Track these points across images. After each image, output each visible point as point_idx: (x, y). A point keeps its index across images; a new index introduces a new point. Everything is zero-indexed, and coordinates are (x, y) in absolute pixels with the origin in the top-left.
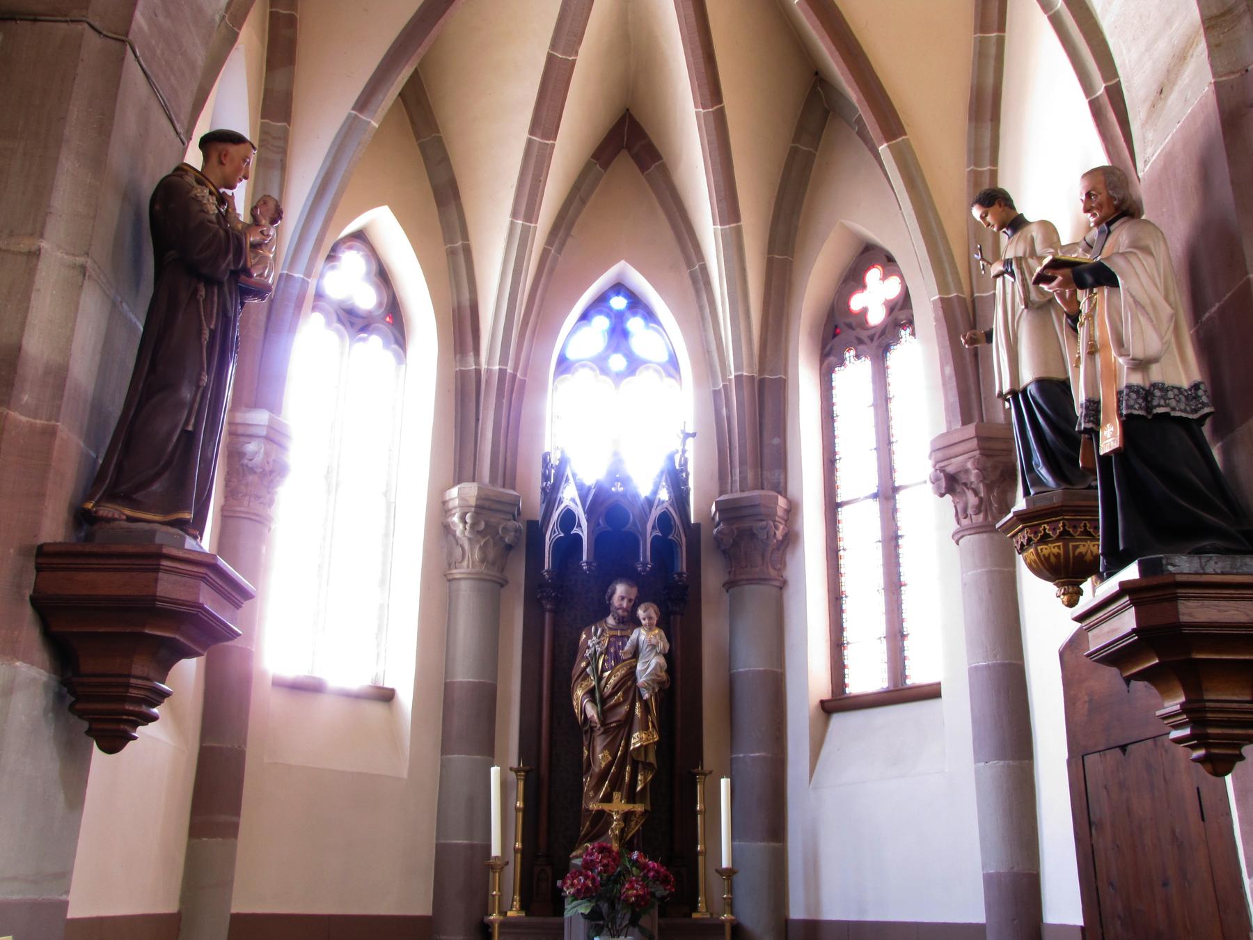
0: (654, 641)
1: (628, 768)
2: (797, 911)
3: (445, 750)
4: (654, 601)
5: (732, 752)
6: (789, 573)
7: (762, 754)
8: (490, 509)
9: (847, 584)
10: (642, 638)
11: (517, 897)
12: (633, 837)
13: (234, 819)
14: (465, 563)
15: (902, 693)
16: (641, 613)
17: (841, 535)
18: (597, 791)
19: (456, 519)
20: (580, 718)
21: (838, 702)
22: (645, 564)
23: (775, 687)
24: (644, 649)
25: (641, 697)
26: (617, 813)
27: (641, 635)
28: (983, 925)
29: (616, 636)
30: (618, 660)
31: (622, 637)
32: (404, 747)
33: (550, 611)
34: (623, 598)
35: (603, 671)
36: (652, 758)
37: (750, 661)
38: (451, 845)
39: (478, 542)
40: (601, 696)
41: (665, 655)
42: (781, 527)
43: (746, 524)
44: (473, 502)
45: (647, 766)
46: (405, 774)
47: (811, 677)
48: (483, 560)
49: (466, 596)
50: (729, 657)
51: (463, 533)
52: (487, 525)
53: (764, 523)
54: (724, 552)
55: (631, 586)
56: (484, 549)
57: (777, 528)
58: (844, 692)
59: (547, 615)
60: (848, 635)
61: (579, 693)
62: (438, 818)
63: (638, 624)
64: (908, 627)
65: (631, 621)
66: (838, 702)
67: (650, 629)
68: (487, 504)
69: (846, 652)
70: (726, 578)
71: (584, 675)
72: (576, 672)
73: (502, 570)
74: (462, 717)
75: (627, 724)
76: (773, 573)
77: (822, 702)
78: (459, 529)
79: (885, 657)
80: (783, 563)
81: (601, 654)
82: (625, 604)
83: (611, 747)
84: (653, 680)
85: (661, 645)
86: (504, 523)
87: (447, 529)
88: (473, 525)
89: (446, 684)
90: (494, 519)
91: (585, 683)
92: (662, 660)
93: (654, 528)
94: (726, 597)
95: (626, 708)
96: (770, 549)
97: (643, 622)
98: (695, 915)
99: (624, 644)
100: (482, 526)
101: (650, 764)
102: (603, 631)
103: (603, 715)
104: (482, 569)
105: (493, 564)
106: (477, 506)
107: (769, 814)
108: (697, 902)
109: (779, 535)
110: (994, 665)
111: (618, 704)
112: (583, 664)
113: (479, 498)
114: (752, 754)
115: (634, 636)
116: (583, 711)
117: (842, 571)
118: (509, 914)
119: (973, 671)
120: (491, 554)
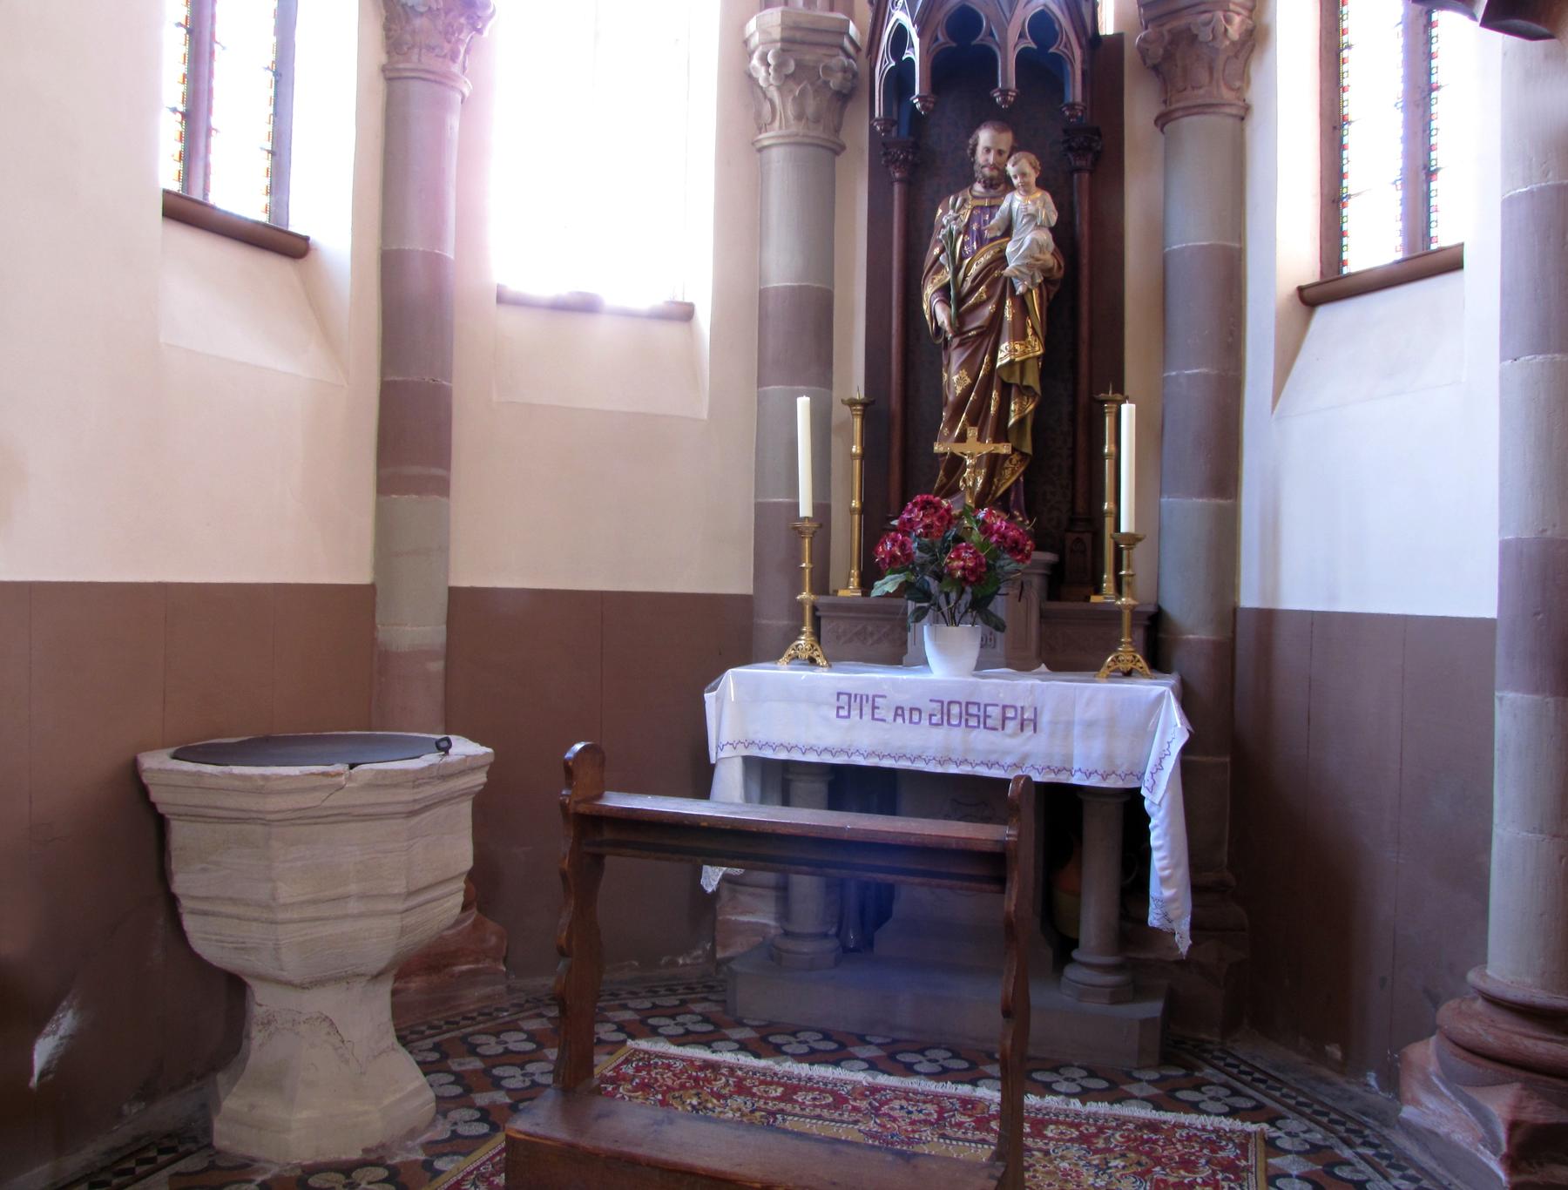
0: (1031, 209)
1: (995, 394)
2: (1249, 599)
3: (760, 383)
4: (1039, 157)
5: (1165, 364)
6: (1254, 95)
7: (1203, 370)
8: (803, 43)
9: (1353, 104)
10: (1016, 205)
11: (855, 572)
12: (1007, 491)
13: (440, 472)
14: (777, 124)
15: (1428, 263)
16: (1011, 169)
17: (1345, 25)
18: (952, 430)
19: (755, 61)
20: (932, 327)
21: (1332, 287)
22: (1004, 93)
23: (1229, 272)
24: (1020, 221)
25: (1013, 290)
26: (971, 455)
27: (1016, 202)
28: (1492, 621)
29: (982, 208)
30: (981, 241)
31: (991, 207)
32: (702, 380)
33: (900, 181)
34: (988, 150)
35: (962, 258)
36: (1032, 380)
37: (1191, 232)
38: (769, 504)
39: (791, 91)
40: (958, 293)
41: (1052, 230)
42: (1237, 20)
43: (1179, 23)
44: (777, 34)
45: (1024, 390)
46: (705, 415)
47: (1287, 251)
48: (800, 116)
49: (780, 166)
50: (1159, 230)
51: (767, 79)
52: (799, 65)
53: (1207, 16)
54: (1156, 69)
55: (1001, 130)
56: (800, 101)
57: (1228, 21)
58: (1340, 271)
59: (896, 188)
60: (1350, 185)
61: (929, 290)
62: (756, 471)
63: (1010, 187)
64: (1439, 157)
65: (1000, 183)
66: (1332, 287)
67: (1027, 192)
68: (798, 35)
69: (1345, 212)
70: (1162, 108)
71: (937, 267)
72: (928, 263)
73: (837, 130)
74: (794, 334)
75: (993, 329)
76: (1227, 95)
77: (1301, 289)
78: (761, 74)
79: (1398, 210)
80: (1244, 76)
81: (959, 233)
82: (991, 158)
83: (969, 365)
84: (1028, 266)
85: (1042, 215)
86: (827, 61)
87: (751, 78)
88: (780, 66)
89: (761, 292)
90: (809, 57)
91: (938, 277)
92: (1045, 237)
93: (1022, 36)
94: (1161, 137)
95: (990, 308)
96: (1222, 58)
97: (1016, 182)
98: (1095, 599)
99: (991, 217)
100: (791, 67)
101: (1028, 388)
102: (965, 201)
103: (960, 320)
104: (795, 127)
105: (817, 121)
106: (783, 40)
107: (1216, 458)
108: (1101, 581)
109: (1234, 32)
110: (1541, 190)
111: (980, 304)
112: (937, 251)
113: (785, 27)
114: (1191, 372)
115: (1005, 205)
116: (933, 316)
117: (1345, 83)
118: (842, 593)
119: (1508, 203)
120: (811, 107)
